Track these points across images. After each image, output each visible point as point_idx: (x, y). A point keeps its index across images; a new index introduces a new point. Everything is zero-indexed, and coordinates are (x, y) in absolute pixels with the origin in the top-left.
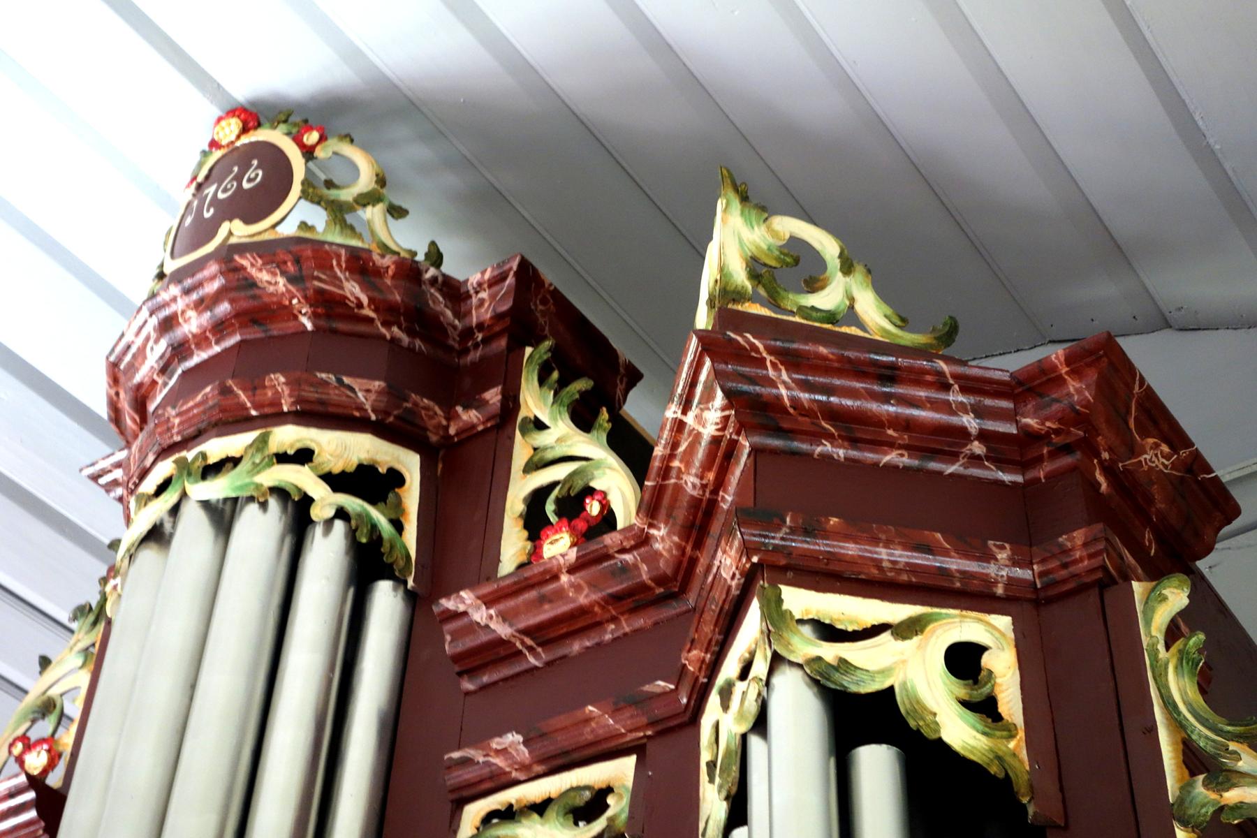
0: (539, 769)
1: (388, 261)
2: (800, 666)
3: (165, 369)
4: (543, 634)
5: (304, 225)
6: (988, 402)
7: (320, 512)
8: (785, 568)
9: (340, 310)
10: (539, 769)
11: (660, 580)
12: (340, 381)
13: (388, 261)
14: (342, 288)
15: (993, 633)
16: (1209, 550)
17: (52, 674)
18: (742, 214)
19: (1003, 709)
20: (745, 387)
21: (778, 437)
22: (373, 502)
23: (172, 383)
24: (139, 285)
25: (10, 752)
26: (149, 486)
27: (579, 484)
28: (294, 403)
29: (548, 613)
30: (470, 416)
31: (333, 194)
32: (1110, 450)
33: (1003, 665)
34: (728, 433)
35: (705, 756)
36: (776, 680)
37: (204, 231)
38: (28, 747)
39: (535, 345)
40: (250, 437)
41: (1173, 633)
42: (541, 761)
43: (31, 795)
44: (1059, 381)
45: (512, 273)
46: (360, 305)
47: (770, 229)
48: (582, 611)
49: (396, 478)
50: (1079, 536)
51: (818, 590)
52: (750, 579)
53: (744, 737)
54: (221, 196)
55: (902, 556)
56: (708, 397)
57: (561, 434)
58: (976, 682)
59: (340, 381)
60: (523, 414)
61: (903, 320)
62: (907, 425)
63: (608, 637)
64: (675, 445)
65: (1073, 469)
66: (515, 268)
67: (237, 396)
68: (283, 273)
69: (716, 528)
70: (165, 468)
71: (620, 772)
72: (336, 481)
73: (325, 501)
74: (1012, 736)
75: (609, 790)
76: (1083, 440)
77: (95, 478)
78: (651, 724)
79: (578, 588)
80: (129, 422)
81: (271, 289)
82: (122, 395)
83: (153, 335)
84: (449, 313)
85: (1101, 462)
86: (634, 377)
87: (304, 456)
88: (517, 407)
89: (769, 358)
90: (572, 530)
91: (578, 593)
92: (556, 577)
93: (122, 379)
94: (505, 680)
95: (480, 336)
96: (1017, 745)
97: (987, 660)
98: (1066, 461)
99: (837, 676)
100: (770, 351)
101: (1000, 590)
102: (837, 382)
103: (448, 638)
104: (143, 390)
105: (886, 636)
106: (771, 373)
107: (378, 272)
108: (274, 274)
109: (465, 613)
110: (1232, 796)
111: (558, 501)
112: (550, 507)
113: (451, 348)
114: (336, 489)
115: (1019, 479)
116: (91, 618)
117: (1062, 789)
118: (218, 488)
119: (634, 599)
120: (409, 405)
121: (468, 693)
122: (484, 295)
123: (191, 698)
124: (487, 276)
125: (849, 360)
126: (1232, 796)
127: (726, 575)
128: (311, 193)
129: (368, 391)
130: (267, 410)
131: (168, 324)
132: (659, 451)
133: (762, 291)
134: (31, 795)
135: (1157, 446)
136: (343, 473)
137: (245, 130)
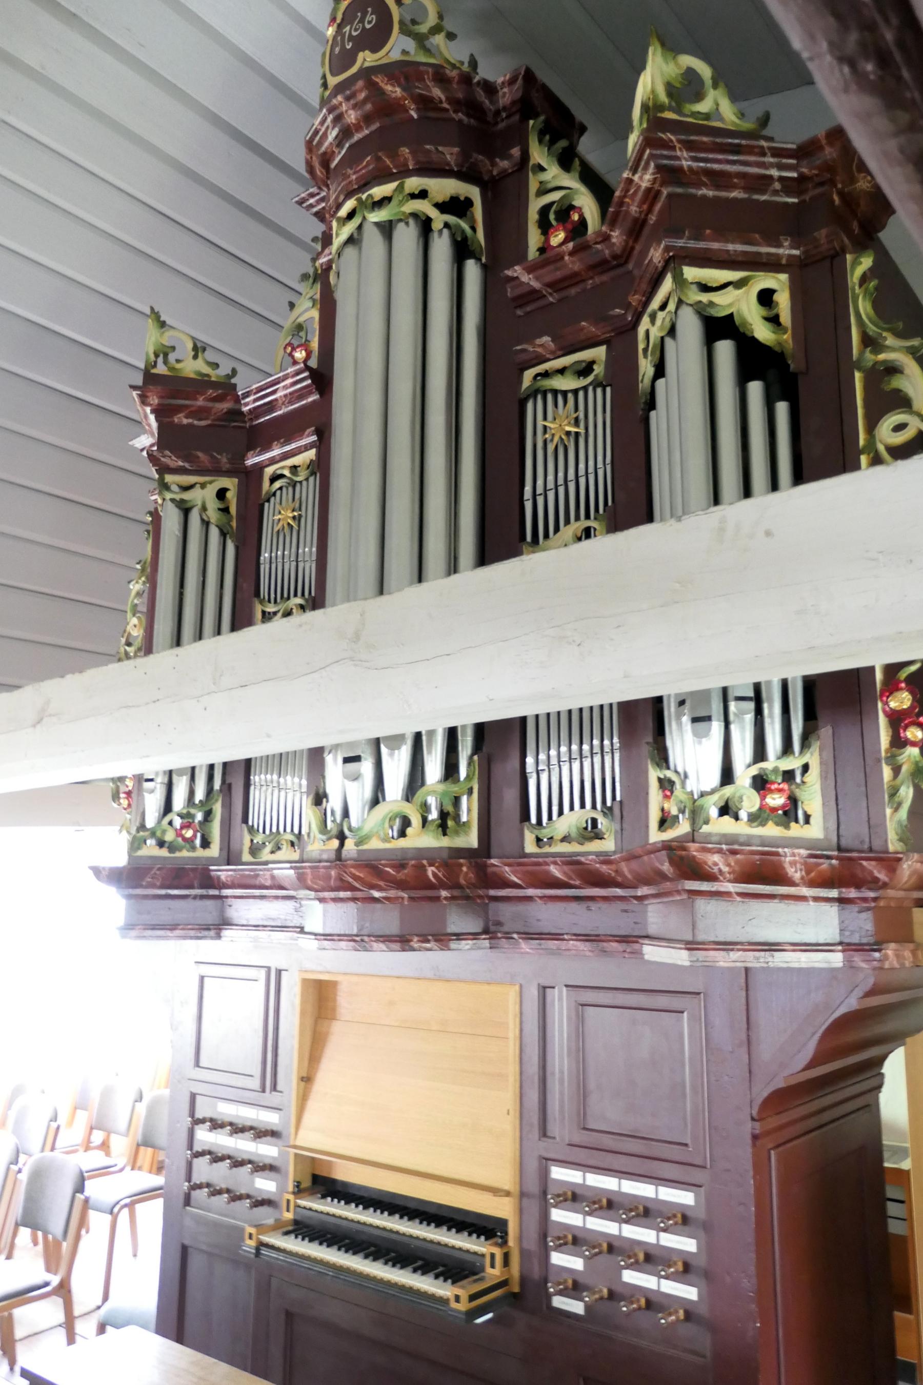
0: (560, 353)
1: (454, 73)
2: (691, 305)
3: (340, 145)
4: (554, 286)
5: (404, 52)
6: (784, 161)
7: (437, 225)
8: (685, 257)
10: (560, 353)
11: (615, 257)
12: (437, 149)
13: (454, 73)
14: (430, 91)
15: (778, 282)
16: (883, 227)
17: (297, 311)
18: (662, 55)
20: (665, 162)
23: (343, 152)
24: (313, 95)
25: (285, 352)
27: (566, 204)
28: (415, 164)
29: (559, 275)
30: (504, 164)
32: (843, 183)
33: (783, 300)
34: (656, 186)
35: (641, 346)
37: (347, 59)
38: (294, 349)
39: (535, 116)
40: (393, 185)
41: (864, 279)
42: (560, 349)
43: (306, 374)
44: (821, 148)
45: (521, 77)
46: (441, 102)
47: (677, 64)
48: (575, 274)
49: (469, 202)
52: (667, 262)
53: (662, 338)
54: (354, 34)
55: (740, 247)
56: (646, 168)
57: (553, 173)
60: (531, 163)
61: (743, 115)
62: (744, 175)
63: (589, 287)
64: (627, 191)
66: (523, 73)
67: (385, 162)
68: (399, 85)
69: (646, 231)
70: (349, 205)
71: (599, 353)
72: (442, 207)
73: (439, 219)
74: (785, 333)
75: (593, 362)
77: (301, 203)
78: (612, 331)
79: (573, 262)
80: (319, 173)
81: (394, 95)
82: (314, 158)
84: (487, 102)
85: (837, 190)
86: (583, 129)
87: (423, 194)
89: (678, 146)
90: (565, 229)
91: (572, 264)
92: (563, 258)
93: (314, 150)
94: (538, 309)
95: (504, 115)
97: (776, 297)
99: (708, 309)
100: (679, 141)
102: (711, 156)
104: (328, 157)
105: (730, 288)
106: (679, 153)
108: (393, 86)
109: (517, 277)
110: (882, 357)
111: (556, 213)
112: (552, 217)
115: (795, 200)
116: (311, 280)
117: (806, 356)
119: (602, 266)
120: (472, 160)
121: (520, 316)
122: (506, 90)
124: (507, 77)
125: (717, 143)
126: (882, 357)
127: (655, 260)
128: (405, 30)
129: (452, 154)
130: (402, 169)
131: (338, 119)
132: (617, 194)
133: (674, 104)
134: (306, 374)
135: (865, 177)
136: (444, 202)
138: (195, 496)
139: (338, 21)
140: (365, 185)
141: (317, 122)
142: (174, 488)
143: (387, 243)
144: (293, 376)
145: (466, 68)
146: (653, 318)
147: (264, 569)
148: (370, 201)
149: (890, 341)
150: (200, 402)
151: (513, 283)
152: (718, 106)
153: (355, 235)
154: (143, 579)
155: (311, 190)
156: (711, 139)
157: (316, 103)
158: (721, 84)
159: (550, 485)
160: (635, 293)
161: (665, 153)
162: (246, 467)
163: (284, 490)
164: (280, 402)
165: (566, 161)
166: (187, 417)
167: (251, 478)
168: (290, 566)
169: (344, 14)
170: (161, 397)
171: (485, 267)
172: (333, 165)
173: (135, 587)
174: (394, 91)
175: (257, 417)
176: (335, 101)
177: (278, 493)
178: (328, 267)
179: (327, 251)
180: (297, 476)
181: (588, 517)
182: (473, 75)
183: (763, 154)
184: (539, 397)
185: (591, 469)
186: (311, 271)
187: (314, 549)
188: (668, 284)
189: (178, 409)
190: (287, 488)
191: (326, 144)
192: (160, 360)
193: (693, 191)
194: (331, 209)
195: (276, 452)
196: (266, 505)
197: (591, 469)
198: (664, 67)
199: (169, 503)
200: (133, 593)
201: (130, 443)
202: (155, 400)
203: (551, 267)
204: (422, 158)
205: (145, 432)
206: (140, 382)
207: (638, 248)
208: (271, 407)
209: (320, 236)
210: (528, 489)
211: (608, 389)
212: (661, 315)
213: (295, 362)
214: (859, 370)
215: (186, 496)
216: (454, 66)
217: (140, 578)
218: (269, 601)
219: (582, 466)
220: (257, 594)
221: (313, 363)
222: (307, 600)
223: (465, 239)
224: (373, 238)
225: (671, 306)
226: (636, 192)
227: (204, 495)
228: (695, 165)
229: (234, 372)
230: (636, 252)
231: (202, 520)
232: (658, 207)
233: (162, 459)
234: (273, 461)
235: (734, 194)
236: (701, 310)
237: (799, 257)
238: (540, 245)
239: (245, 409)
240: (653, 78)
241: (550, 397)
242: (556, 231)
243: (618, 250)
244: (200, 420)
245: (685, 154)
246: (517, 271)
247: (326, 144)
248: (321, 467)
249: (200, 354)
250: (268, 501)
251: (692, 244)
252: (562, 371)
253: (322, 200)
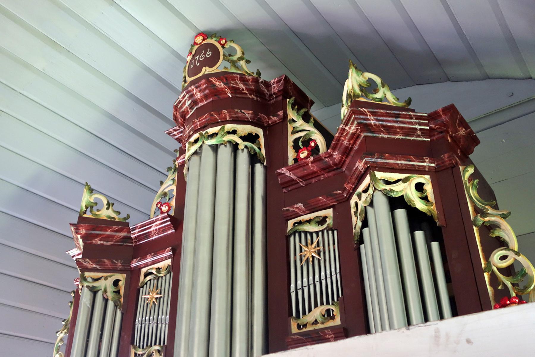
0: (308, 212)
6: (422, 121)
7: (241, 147)
9: (239, 91)
10: (308, 212)
12: (241, 111)
19: (429, 199)
20: (362, 121)
21: (371, 133)
22: (253, 143)
23: (193, 111)
24: (179, 85)
26: (192, 139)
27: (308, 138)
30: (275, 119)
31: (231, 58)
32: (451, 131)
33: (429, 188)
34: (358, 132)
35: (353, 210)
36: (374, 194)
38: (161, 205)
39: (290, 98)
42: (308, 210)
43: (169, 219)
46: (243, 90)
48: (314, 173)
49: (257, 136)
50: (446, 155)
51: (384, 172)
57: (300, 123)
58: (423, 192)
59: (241, 111)
61: (398, 99)
62: (402, 128)
64: (342, 134)
65: (443, 137)
68: (222, 82)
69: (352, 153)
70: (196, 136)
71: (329, 212)
72: (244, 138)
73: (242, 144)
75: (326, 217)
76: (446, 130)
77: (169, 134)
78: (336, 201)
79: (313, 167)
81: (220, 87)
83: (187, 99)
86: (312, 103)
87: (234, 132)
88: (287, 116)
89: (368, 114)
90: (307, 150)
92: (308, 164)
94: (295, 189)
96: (433, 207)
97: (425, 187)
98: (441, 135)
100: (369, 112)
101: (427, 170)
102: (385, 118)
105: (400, 182)
106: (369, 117)
107: (248, 81)
108: (220, 82)
110: (487, 219)
111: (302, 142)
112: (300, 144)
113: (267, 100)
114: (244, 141)
115: (429, 140)
116: (173, 171)
118: (213, 142)
119: (327, 168)
121: (285, 192)
122: (275, 85)
123: (215, 196)
126: (487, 219)
131: (191, 96)
133: (364, 94)
134: (169, 219)
137: (204, 40)
138: (101, 284)
139: (193, 53)
141: (180, 97)
142: (89, 279)
143: (215, 154)
144: (161, 220)
145: (255, 75)
146: (359, 196)
147: (138, 327)
148: (207, 135)
149: (490, 211)
150: (108, 233)
151: (281, 176)
152: (386, 95)
153: (198, 151)
154: (65, 331)
155: (175, 128)
156: (386, 111)
157: (180, 89)
158: (386, 86)
159: (305, 284)
160: (349, 183)
161: (362, 117)
162: (131, 268)
163: (152, 281)
164: (153, 233)
165: (306, 118)
166: (100, 240)
167: (133, 274)
168: (153, 326)
169: (196, 51)
170: (87, 230)
171: (265, 167)
172: (187, 117)
173: (60, 335)
174: (220, 85)
175: (139, 241)
176: (190, 88)
177: (149, 282)
178: (183, 165)
179: (182, 157)
180: (160, 274)
181: (328, 303)
182: (259, 78)
183: (411, 118)
184: (297, 234)
185: (328, 275)
186: (173, 166)
187: (168, 316)
188: (367, 180)
190: (154, 280)
191: (185, 107)
192: (89, 210)
193: (377, 135)
194: (185, 137)
195: (149, 260)
196: (141, 289)
197: (328, 275)
198: (358, 78)
199: (86, 288)
200: (59, 339)
201: (67, 253)
202: (83, 231)
203: (302, 169)
204: (233, 115)
205: (76, 247)
206: (76, 221)
207: (348, 161)
208: (148, 235)
209: (178, 149)
210: (293, 286)
211: (335, 232)
212: (364, 196)
213: (162, 213)
214: (476, 226)
215: (96, 284)
216: (249, 75)
217: (63, 330)
218: (139, 347)
219: (323, 274)
220: (133, 343)
221: (172, 213)
222: (162, 348)
223: (256, 153)
224: (208, 153)
225: (371, 191)
226: (347, 134)
227: (106, 284)
228: (377, 123)
229: (128, 216)
230: (347, 163)
231: (104, 298)
232: (359, 142)
233: (84, 263)
234: (146, 265)
235: (398, 137)
236: (385, 193)
237: (435, 167)
238: (295, 157)
239: (133, 236)
240: (353, 82)
241: (303, 234)
242: (303, 150)
243: (337, 161)
245: (372, 117)
246: (284, 170)
247: (185, 107)
248: (175, 269)
249: (110, 207)
250: (143, 287)
251: (379, 160)
252: (309, 221)
253: (181, 132)
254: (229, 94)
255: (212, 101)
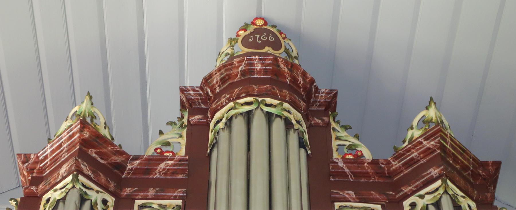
0: (358, 201)
1: (310, 77)
10: (358, 201)
30: (319, 121)
40: (278, 102)
42: (358, 198)
57: (343, 133)
60: (332, 127)
62: (462, 162)
63: (371, 180)
78: (388, 199)
79: (369, 168)
92: (364, 163)
103: (331, 167)
107: (307, 77)
109: (338, 163)
140: (239, 97)
166: (96, 153)
176: (253, 57)
188: (439, 183)
189: (93, 147)
225: (441, 191)
233: (82, 166)
244: (102, 158)
254: (288, 80)
255: (271, 78)
